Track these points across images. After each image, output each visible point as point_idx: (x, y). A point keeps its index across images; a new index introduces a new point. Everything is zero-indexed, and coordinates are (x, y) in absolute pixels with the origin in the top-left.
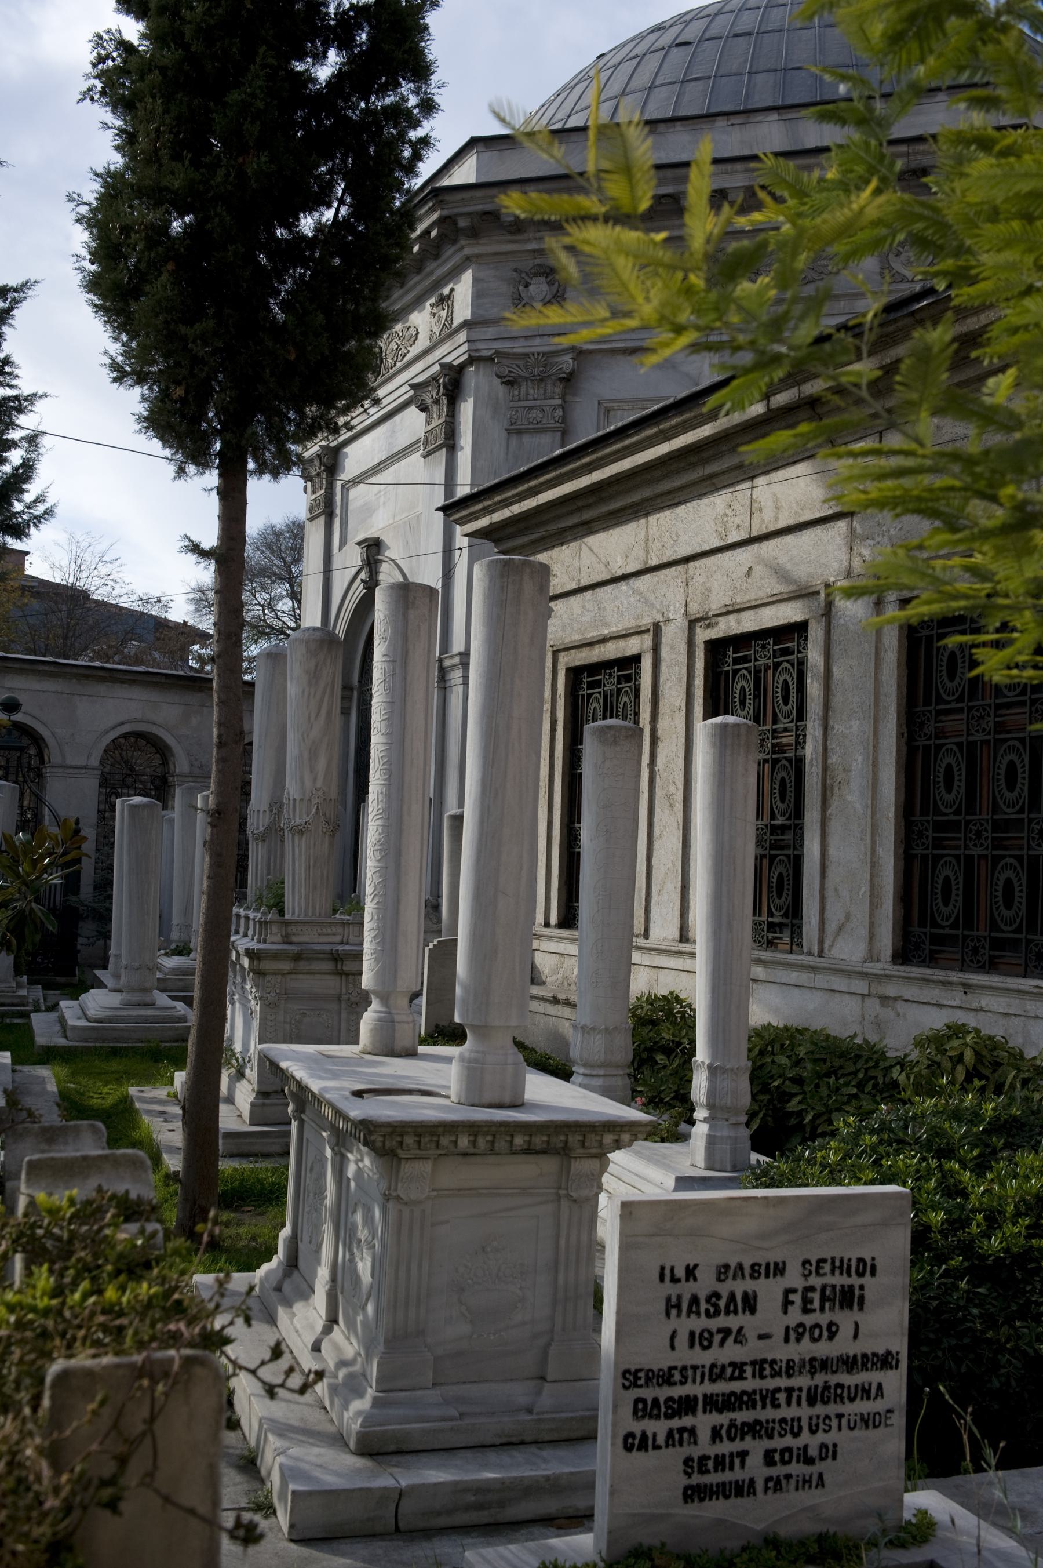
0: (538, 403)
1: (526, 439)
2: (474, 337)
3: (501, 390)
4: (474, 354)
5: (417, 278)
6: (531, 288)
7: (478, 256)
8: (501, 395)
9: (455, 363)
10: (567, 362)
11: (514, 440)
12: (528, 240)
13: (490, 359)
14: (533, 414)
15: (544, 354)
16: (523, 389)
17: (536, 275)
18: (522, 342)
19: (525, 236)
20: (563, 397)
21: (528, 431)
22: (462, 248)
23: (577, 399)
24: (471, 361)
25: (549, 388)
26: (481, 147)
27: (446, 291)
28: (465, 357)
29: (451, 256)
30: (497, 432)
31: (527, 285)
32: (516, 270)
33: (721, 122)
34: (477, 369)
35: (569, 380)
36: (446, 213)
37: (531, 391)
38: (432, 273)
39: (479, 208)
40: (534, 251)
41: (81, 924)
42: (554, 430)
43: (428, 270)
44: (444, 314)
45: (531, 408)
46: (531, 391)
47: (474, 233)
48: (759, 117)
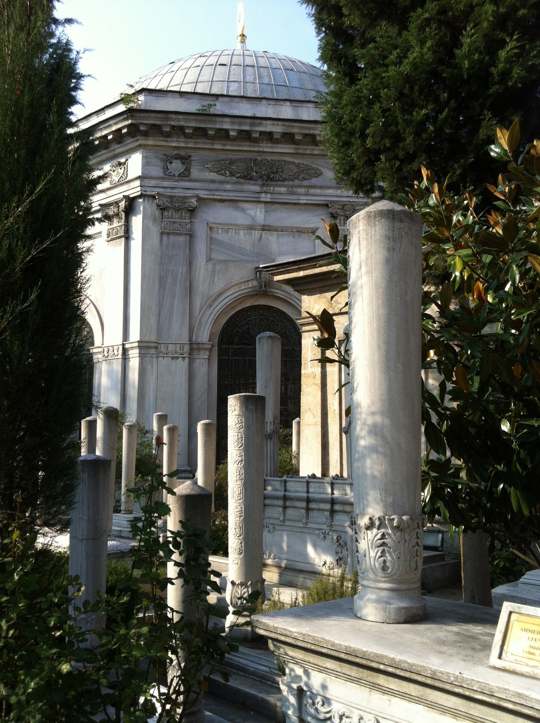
0: (178, 220)
1: (172, 237)
2: (144, 184)
3: (158, 213)
4: (143, 193)
5: (104, 152)
6: (173, 164)
7: (145, 145)
8: (157, 214)
9: (131, 196)
10: (194, 202)
11: (165, 237)
12: (173, 141)
13: (153, 197)
14: (176, 225)
15: (181, 197)
16: (170, 213)
17: (176, 158)
18: (169, 190)
19: (172, 139)
20: (190, 218)
21: (173, 234)
22: (138, 140)
23: (196, 221)
24: (140, 196)
25: (184, 214)
26: (146, 92)
27: (123, 160)
28: (139, 193)
29: (130, 143)
30: (155, 231)
31: (171, 163)
32: (165, 155)
33: (264, 102)
34: (144, 200)
35: (192, 211)
36: (134, 122)
37: (174, 214)
38: (114, 150)
39: (152, 122)
40: (175, 147)
41: (265, 533)
42: (186, 234)
43: (112, 148)
44: (121, 171)
45: (174, 222)
46: (174, 214)
47: (146, 134)
48: (282, 103)
